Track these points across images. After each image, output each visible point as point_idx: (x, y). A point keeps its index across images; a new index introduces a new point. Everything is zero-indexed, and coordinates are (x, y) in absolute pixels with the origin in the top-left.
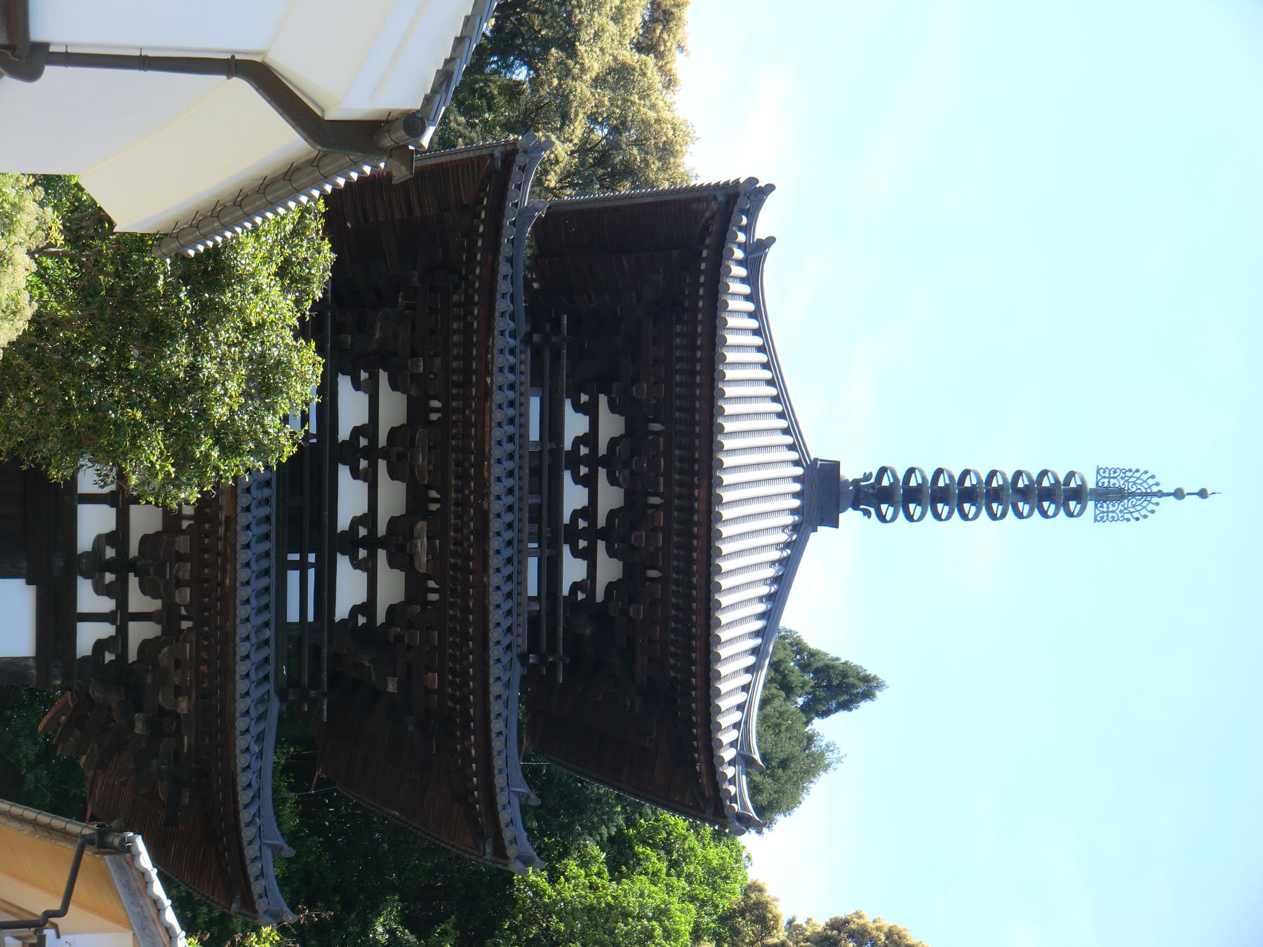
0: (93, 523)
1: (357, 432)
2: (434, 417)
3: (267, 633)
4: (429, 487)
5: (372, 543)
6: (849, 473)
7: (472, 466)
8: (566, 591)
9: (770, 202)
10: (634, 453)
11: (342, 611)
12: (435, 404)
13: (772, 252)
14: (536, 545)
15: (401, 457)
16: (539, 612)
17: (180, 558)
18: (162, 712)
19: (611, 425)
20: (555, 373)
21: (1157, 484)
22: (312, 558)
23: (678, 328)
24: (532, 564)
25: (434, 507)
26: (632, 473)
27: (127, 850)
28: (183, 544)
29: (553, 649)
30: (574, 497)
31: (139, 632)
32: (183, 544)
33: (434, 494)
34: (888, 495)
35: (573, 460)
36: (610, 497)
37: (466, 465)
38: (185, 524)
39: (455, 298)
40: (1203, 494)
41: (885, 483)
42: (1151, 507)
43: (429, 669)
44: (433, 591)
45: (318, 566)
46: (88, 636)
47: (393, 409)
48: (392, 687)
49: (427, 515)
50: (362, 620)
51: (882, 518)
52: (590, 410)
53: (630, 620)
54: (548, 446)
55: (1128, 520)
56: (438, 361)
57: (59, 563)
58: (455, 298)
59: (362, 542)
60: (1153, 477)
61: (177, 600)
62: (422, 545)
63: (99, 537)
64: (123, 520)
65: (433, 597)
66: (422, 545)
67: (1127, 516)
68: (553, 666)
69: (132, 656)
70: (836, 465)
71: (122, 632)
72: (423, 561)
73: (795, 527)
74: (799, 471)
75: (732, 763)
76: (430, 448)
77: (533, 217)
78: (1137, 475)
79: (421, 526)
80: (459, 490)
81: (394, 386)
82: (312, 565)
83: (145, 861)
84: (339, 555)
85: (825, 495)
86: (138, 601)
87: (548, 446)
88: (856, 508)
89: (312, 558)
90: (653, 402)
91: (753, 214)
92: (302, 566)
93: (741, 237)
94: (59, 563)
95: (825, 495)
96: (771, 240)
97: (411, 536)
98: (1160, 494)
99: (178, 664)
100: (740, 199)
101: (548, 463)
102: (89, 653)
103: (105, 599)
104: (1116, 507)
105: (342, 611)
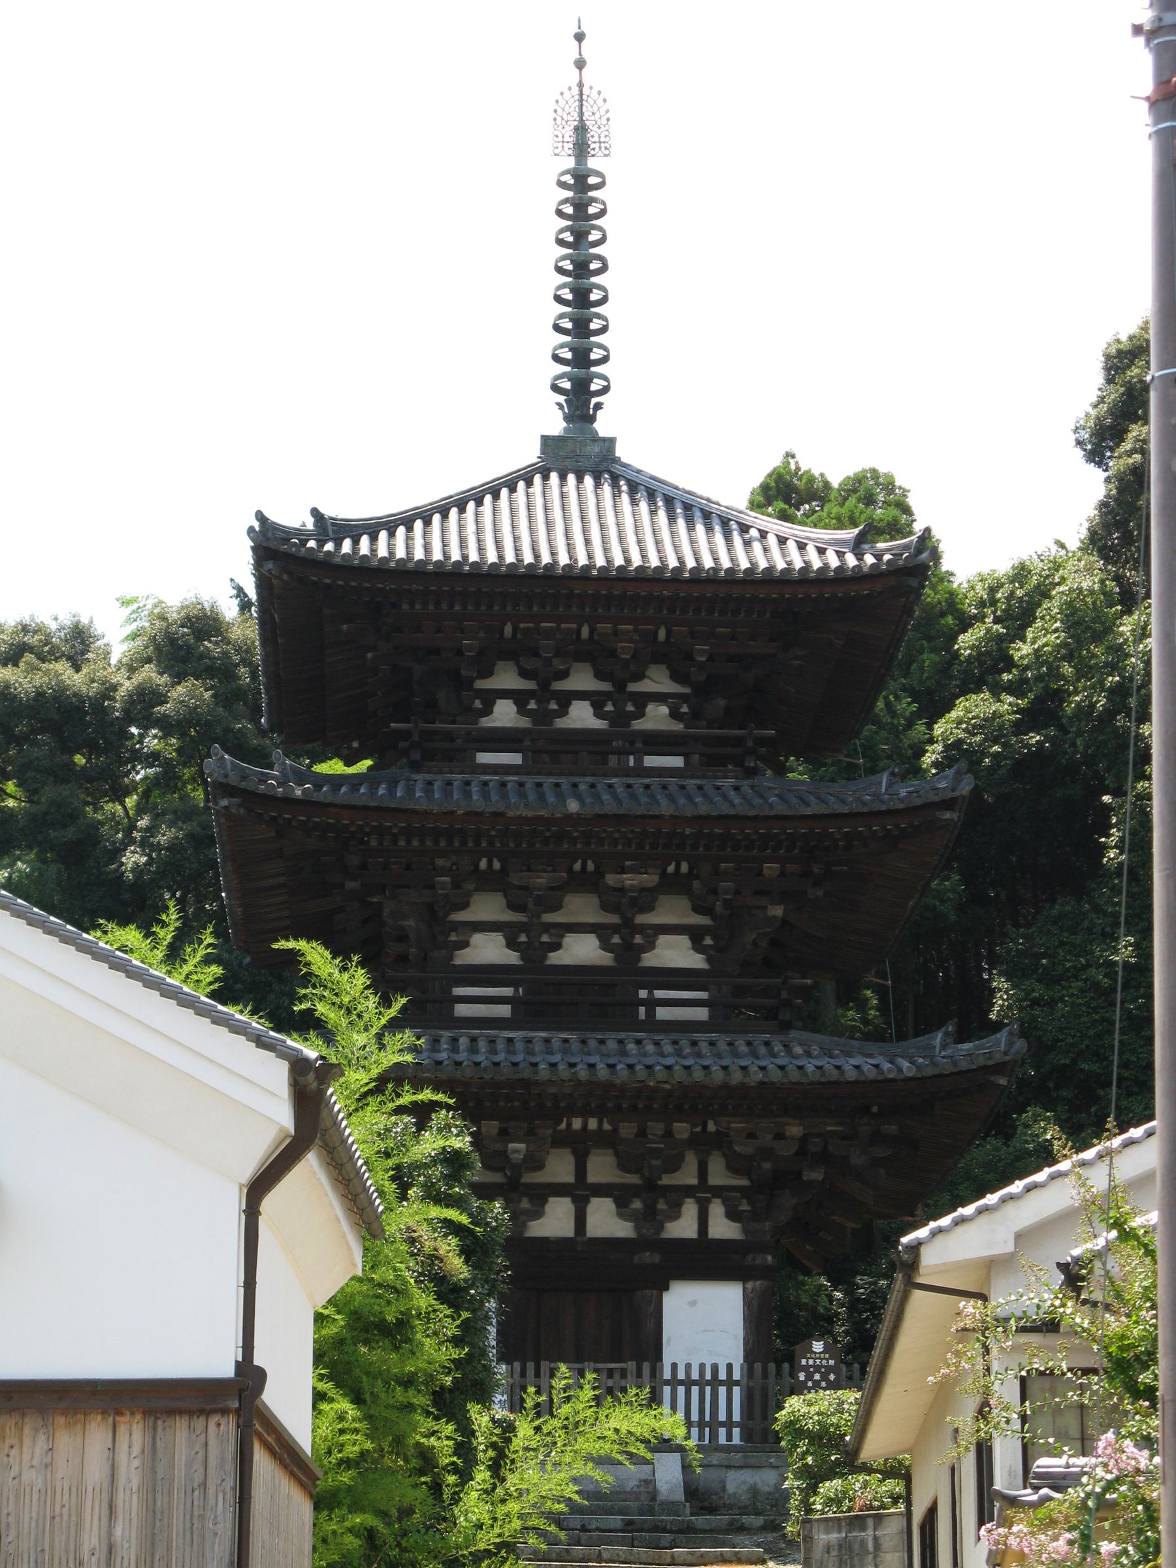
0: (606, 1221)
1: (511, 944)
2: (497, 865)
3: (722, 1046)
4: (570, 870)
5: (628, 927)
6: (556, 425)
7: (549, 830)
8: (678, 727)
9: (274, 516)
10: (535, 653)
11: (697, 961)
12: (483, 864)
13: (328, 511)
14: (631, 758)
15: (539, 901)
16: (701, 755)
17: (642, 1133)
18: (802, 1151)
19: (507, 678)
20: (449, 737)
21: (570, 89)
22: (643, 994)
23: (405, 606)
24: (651, 761)
25: (591, 866)
26: (556, 655)
27: (915, 1248)
28: (628, 1130)
29: (738, 742)
30: (582, 716)
31: (718, 1175)
32: (628, 1130)
33: (577, 866)
34: (580, 396)
35: (543, 718)
36: (582, 679)
37: (548, 834)
38: (607, 1126)
39: (374, 843)
40: (580, 37)
41: (567, 385)
42: (594, 95)
43: (760, 873)
44: (678, 867)
45: (651, 987)
46: (722, 1228)
47: (487, 907)
48: (777, 911)
49: (599, 873)
50: (708, 941)
51: (605, 390)
52: (490, 698)
53: (710, 659)
54: (527, 743)
55: (608, 120)
56: (439, 862)
57: (649, 1257)
58: (374, 843)
59: (627, 939)
60: (562, 94)
61: (686, 1136)
62: (630, 880)
63: (620, 1215)
64: (601, 1190)
65: (684, 867)
66: (630, 880)
67: (604, 121)
68: (760, 741)
69: (744, 1182)
70: (545, 440)
71: (719, 1192)
72: (649, 879)
73: (615, 480)
74: (554, 477)
75: (859, 556)
76: (529, 870)
77: (291, 766)
78: (560, 111)
79: (611, 879)
80: (574, 841)
81: (465, 906)
82: (651, 993)
83: (922, 1233)
84: (640, 964)
85: (579, 451)
86: (688, 1176)
87: (527, 743)
88: (593, 419)
89: (643, 994)
90: (482, 634)
91: (285, 534)
92: (652, 1004)
93: (312, 544)
94: (649, 1257)
95: (579, 451)
96: (315, 513)
97: (622, 890)
98: (581, 85)
99: (752, 1136)
100: (272, 547)
101: (547, 747)
102: (738, 1225)
103: (684, 1209)
104: (594, 135)
105: (697, 961)
